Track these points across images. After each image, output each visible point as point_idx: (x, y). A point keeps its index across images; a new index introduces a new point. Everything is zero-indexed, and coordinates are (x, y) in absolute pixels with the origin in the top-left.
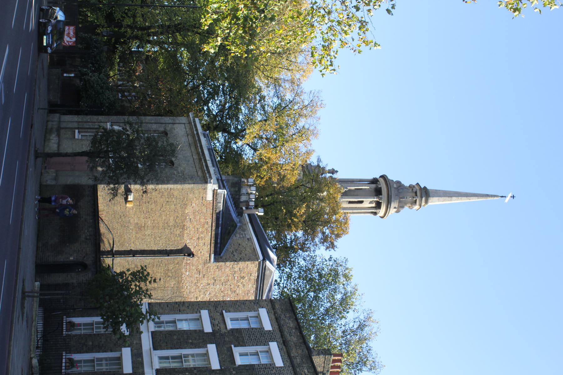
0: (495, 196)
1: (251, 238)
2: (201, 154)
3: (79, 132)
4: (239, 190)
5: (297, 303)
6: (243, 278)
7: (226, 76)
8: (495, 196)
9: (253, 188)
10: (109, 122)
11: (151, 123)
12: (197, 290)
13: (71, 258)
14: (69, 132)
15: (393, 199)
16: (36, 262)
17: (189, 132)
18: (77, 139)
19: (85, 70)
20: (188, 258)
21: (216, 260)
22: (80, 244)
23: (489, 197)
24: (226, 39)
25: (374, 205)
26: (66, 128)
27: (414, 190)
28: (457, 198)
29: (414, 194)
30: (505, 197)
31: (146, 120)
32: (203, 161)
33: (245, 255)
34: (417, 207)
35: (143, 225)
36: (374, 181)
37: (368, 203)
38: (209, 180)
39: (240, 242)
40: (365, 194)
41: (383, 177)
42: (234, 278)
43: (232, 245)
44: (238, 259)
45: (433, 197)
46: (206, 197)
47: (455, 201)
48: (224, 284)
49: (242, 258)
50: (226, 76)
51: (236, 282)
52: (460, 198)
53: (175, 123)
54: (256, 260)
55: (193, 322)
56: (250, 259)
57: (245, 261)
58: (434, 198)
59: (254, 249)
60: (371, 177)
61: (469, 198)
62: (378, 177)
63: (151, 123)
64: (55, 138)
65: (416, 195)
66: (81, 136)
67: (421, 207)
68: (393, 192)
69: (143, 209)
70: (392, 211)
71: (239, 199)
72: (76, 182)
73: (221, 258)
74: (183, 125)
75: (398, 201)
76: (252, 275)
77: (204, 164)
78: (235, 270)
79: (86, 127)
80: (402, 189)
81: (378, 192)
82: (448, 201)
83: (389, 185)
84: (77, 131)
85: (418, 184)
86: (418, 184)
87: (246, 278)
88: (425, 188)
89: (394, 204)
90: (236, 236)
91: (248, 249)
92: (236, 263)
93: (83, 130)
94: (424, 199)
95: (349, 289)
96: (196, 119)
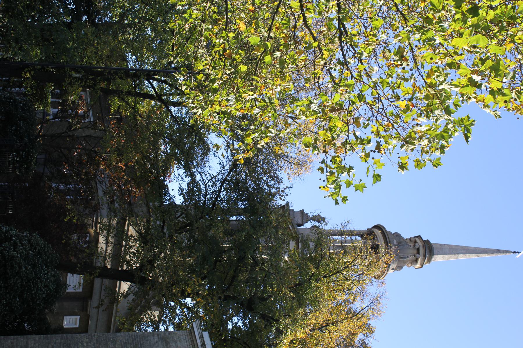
7: (66, 220)
9: (137, 157)
23: (501, 253)
24: (440, 20)
27: (417, 246)
29: (415, 251)
34: (418, 266)
36: (370, 232)
45: (438, 254)
50: (66, 220)
52: (467, 255)
61: (478, 254)
65: (418, 253)
80: (402, 245)
86: (419, 237)
96: (204, 333)
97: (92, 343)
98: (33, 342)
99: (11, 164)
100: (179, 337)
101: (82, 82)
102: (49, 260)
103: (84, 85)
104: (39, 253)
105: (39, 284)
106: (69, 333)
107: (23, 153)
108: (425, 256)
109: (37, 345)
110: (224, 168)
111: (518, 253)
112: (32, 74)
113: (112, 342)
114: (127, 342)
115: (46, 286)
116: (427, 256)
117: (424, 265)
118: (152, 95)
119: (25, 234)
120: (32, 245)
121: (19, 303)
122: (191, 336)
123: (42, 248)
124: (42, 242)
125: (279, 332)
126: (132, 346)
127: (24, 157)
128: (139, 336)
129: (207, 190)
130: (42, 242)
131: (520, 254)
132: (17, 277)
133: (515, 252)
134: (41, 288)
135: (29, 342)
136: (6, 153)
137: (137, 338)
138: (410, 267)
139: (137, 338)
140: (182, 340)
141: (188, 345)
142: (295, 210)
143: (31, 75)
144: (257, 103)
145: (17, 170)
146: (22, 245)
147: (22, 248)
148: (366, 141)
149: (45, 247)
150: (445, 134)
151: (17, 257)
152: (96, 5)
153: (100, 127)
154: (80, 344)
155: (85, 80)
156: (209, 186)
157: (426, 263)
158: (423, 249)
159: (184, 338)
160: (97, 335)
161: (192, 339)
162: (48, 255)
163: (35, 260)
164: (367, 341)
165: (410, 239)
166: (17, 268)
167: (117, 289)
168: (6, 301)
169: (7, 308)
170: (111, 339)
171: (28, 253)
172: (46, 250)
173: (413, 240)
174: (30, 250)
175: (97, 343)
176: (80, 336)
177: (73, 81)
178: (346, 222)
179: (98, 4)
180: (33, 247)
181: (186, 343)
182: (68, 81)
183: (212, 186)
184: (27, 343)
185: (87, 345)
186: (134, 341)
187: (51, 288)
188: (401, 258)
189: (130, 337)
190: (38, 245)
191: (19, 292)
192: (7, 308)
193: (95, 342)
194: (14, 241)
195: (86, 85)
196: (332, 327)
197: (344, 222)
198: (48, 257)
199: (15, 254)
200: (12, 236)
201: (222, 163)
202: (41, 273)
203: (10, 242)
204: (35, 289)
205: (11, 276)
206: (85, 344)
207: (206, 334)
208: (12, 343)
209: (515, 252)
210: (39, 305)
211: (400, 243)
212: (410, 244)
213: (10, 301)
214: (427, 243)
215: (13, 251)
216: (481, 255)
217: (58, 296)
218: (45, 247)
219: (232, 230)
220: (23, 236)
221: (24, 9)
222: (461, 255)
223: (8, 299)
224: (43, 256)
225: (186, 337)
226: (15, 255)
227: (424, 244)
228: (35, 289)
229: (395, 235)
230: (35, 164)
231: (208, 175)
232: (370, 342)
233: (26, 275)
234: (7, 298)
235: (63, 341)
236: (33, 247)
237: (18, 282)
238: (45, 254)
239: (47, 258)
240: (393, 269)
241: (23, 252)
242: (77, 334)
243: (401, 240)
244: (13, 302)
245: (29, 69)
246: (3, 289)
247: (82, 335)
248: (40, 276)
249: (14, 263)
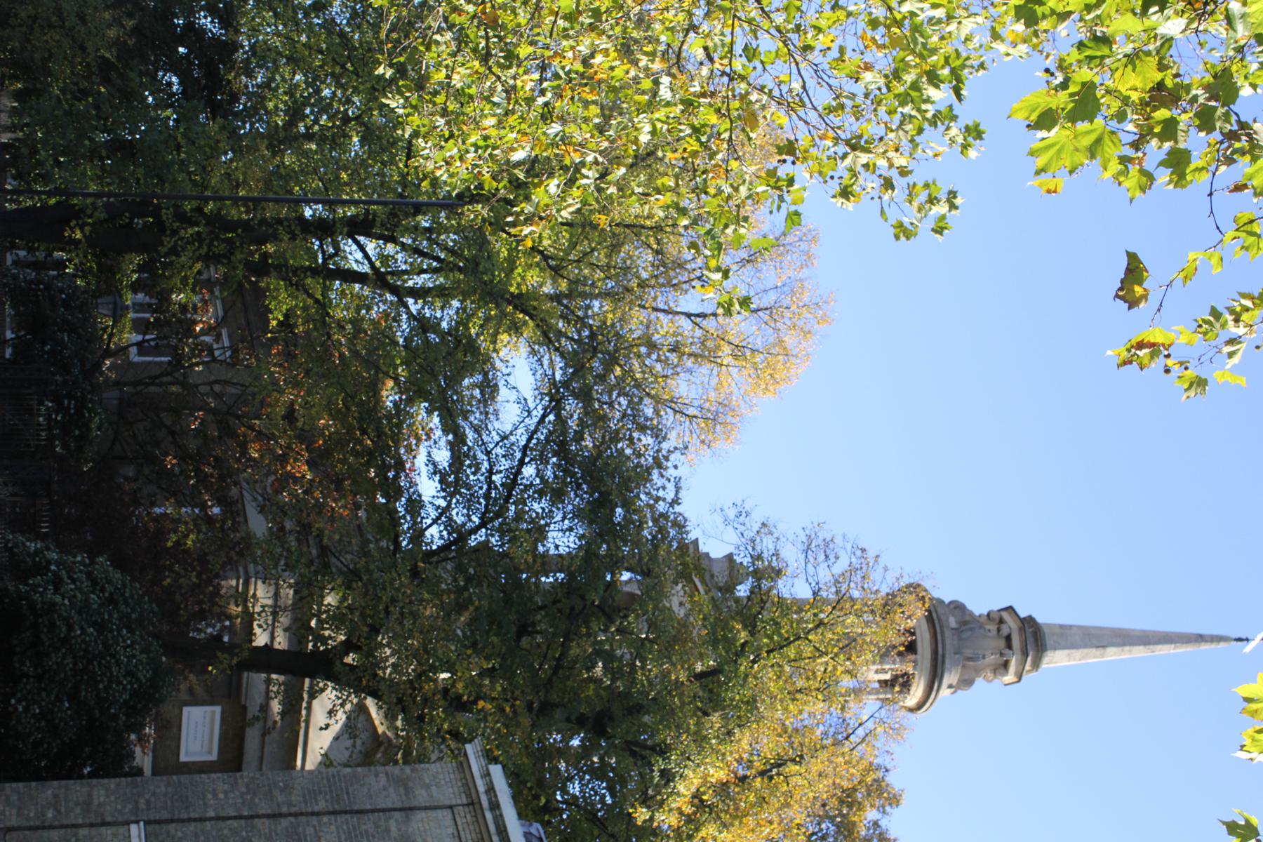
10: (137, 822)
11: (313, 814)
15: (947, 665)
19: (32, 546)
23: (1206, 641)
27: (1005, 631)
28: (1120, 649)
29: (1002, 643)
30: (1247, 640)
34: (1010, 677)
45: (1055, 649)
52: (1127, 648)
53: (411, 809)
58: (1057, 652)
61: (1151, 647)
63: (313, 814)
65: (1009, 646)
67: (1019, 681)
68: (950, 642)
74: (447, 813)
75: (960, 667)
80: (971, 629)
82: (1095, 657)
83: (936, 622)
89: (950, 678)
97: (237, 793)
98: (102, 792)
99: (42, 430)
100: (435, 777)
101: (200, 246)
102: (134, 616)
103: (207, 254)
104: (111, 600)
105: (115, 670)
106: (183, 773)
107: (69, 404)
108: (1025, 654)
109: (113, 798)
110: (529, 412)
111: (1247, 640)
112: (88, 234)
113: (282, 790)
114: (316, 788)
115: (129, 673)
116: (1031, 654)
117: (1024, 677)
118: (366, 274)
119: (79, 559)
120: (94, 583)
121: (69, 712)
122: (462, 775)
123: (119, 589)
124: (118, 576)
125: (667, 776)
126: (328, 797)
127: (72, 411)
128: (344, 777)
129: (491, 466)
130: (117, 576)
131: (1252, 645)
132: (64, 650)
133: (1240, 640)
134: (117, 677)
135: (95, 793)
136: (31, 400)
137: (340, 780)
138: (991, 681)
139: (340, 780)
140: (443, 782)
141: (457, 793)
142: (713, 555)
143: (84, 235)
145: (57, 442)
146: (74, 581)
147: (73, 587)
148: (784, 180)
149: (124, 586)
150: (914, 94)
151: (64, 604)
152: (229, 82)
153: (247, 360)
154: (210, 796)
155: (207, 241)
156: (497, 455)
157: (1029, 671)
158: (1021, 635)
159: (448, 780)
160: (248, 776)
161: (464, 781)
162: (132, 604)
163: (103, 614)
164: (884, 823)
165: (988, 615)
166: (64, 629)
167: (299, 763)
168: (40, 707)
169: (43, 723)
170: (281, 784)
171: (87, 600)
172: (127, 595)
173: (996, 616)
174: (93, 592)
175: (248, 793)
176: (209, 778)
177: (180, 243)
178: (816, 524)
179: (235, 78)
180: (98, 588)
181: (451, 790)
182: (169, 242)
183: (503, 456)
184: (90, 795)
185: (226, 797)
186: (333, 788)
187: (142, 677)
188: (969, 659)
189: (323, 778)
190: (109, 581)
191: (70, 685)
192: (43, 723)
193: (244, 789)
194: (55, 574)
195: (211, 254)
196: (794, 768)
197: (810, 526)
198: (133, 611)
199: (58, 599)
200: (49, 563)
201: (523, 402)
202: (118, 645)
203: (47, 575)
204: (105, 679)
205: (51, 649)
206: (221, 796)
207: (496, 771)
208: (55, 796)
209: (1240, 640)
210: (115, 717)
211: (965, 623)
212: (988, 627)
213: (50, 706)
214: (1029, 624)
215: (54, 594)
216: (1159, 647)
217: (157, 696)
218: (124, 586)
220: (74, 563)
221: (64, 94)
222: (1111, 650)
223: (43, 704)
224: (122, 607)
225: (452, 776)
226: (57, 600)
227: (1020, 623)
228: (105, 679)
229: (952, 606)
230: (99, 428)
231: (494, 433)
232: (894, 823)
233: (83, 646)
234: (43, 700)
235: (170, 789)
236: (98, 588)
237: (66, 662)
238: (126, 603)
239: (129, 611)
240: (950, 686)
241: (75, 596)
242: (203, 776)
243: (967, 618)
244: (56, 710)
245: (80, 222)
246: (31, 680)
247: (214, 776)
248: (115, 650)
249: (56, 616)
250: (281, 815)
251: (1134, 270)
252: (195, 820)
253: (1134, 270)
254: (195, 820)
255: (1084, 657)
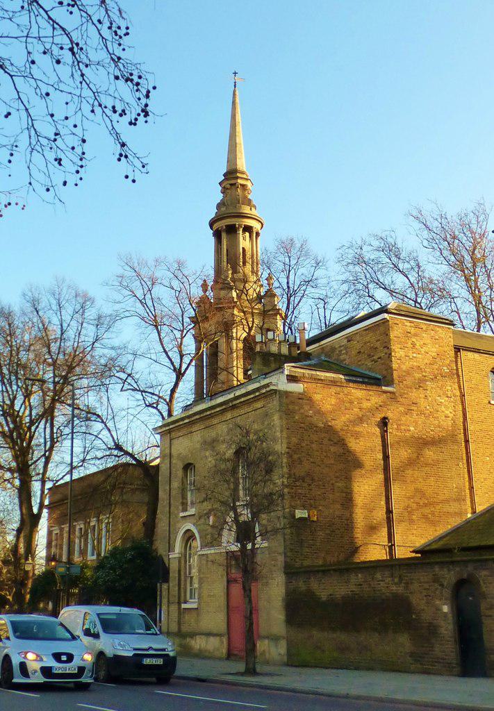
0: (234, 94)
1: (347, 337)
2: (224, 407)
3: (185, 603)
4: (273, 355)
5: (98, 578)
6: (414, 345)
8: (234, 94)
12: (435, 415)
13: (446, 609)
14: (186, 618)
16: (459, 676)
17: (184, 431)
18: (199, 604)
20: (389, 426)
21: (390, 382)
22: (411, 593)
25: (247, 234)
26: (179, 624)
31: (165, 497)
32: (238, 401)
33: (379, 342)
34: (248, 183)
35: (344, 495)
36: (217, 235)
37: (244, 242)
38: (272, 387)
39: (354, 352)
40: (234, 244)
41: (211, 224)
42: (415, 357)
43: (359, 363)
44: (386, 350)
46: (300, 394)
47: (240, 139)
48: (424, 374)
49: (383, 346)
51: (420, 356)
54: (387, 323)
55: (58, 637)
56: (385, 333)
57: (390, 340)
59: (366, 330)
60: (211, 241)
62: (212, 232)
64: (198, 641)
66: (191, 598)
68: (232, 210)
69: (319, 493)
70: (254, 212)
71: (285, 356)
72: (280, 604)
73: (385, 377)
75: (243, 206)
76: (409, 331)
77: (243, 399)
78: (403, 356)
79: (177, 592)
81: (232, 230)
84: (183, 606)
85: (220, 184)
86: (220, 184)
87: (414, 340)
88: (225, 175)
89: (246, 210)
90: (345, 360)
91: (367, 339)
92: (393, 354)
93: (182, 595)
94: (239, 175)
95: (376, 243)
108: (238, 178)
144: (365, 284)
219: (189, 451)
250: (170, 503)
251: (6, 116)
252: (169, 534)
253: (6, 116)
254: (169, 534)
255: (241, 152)
